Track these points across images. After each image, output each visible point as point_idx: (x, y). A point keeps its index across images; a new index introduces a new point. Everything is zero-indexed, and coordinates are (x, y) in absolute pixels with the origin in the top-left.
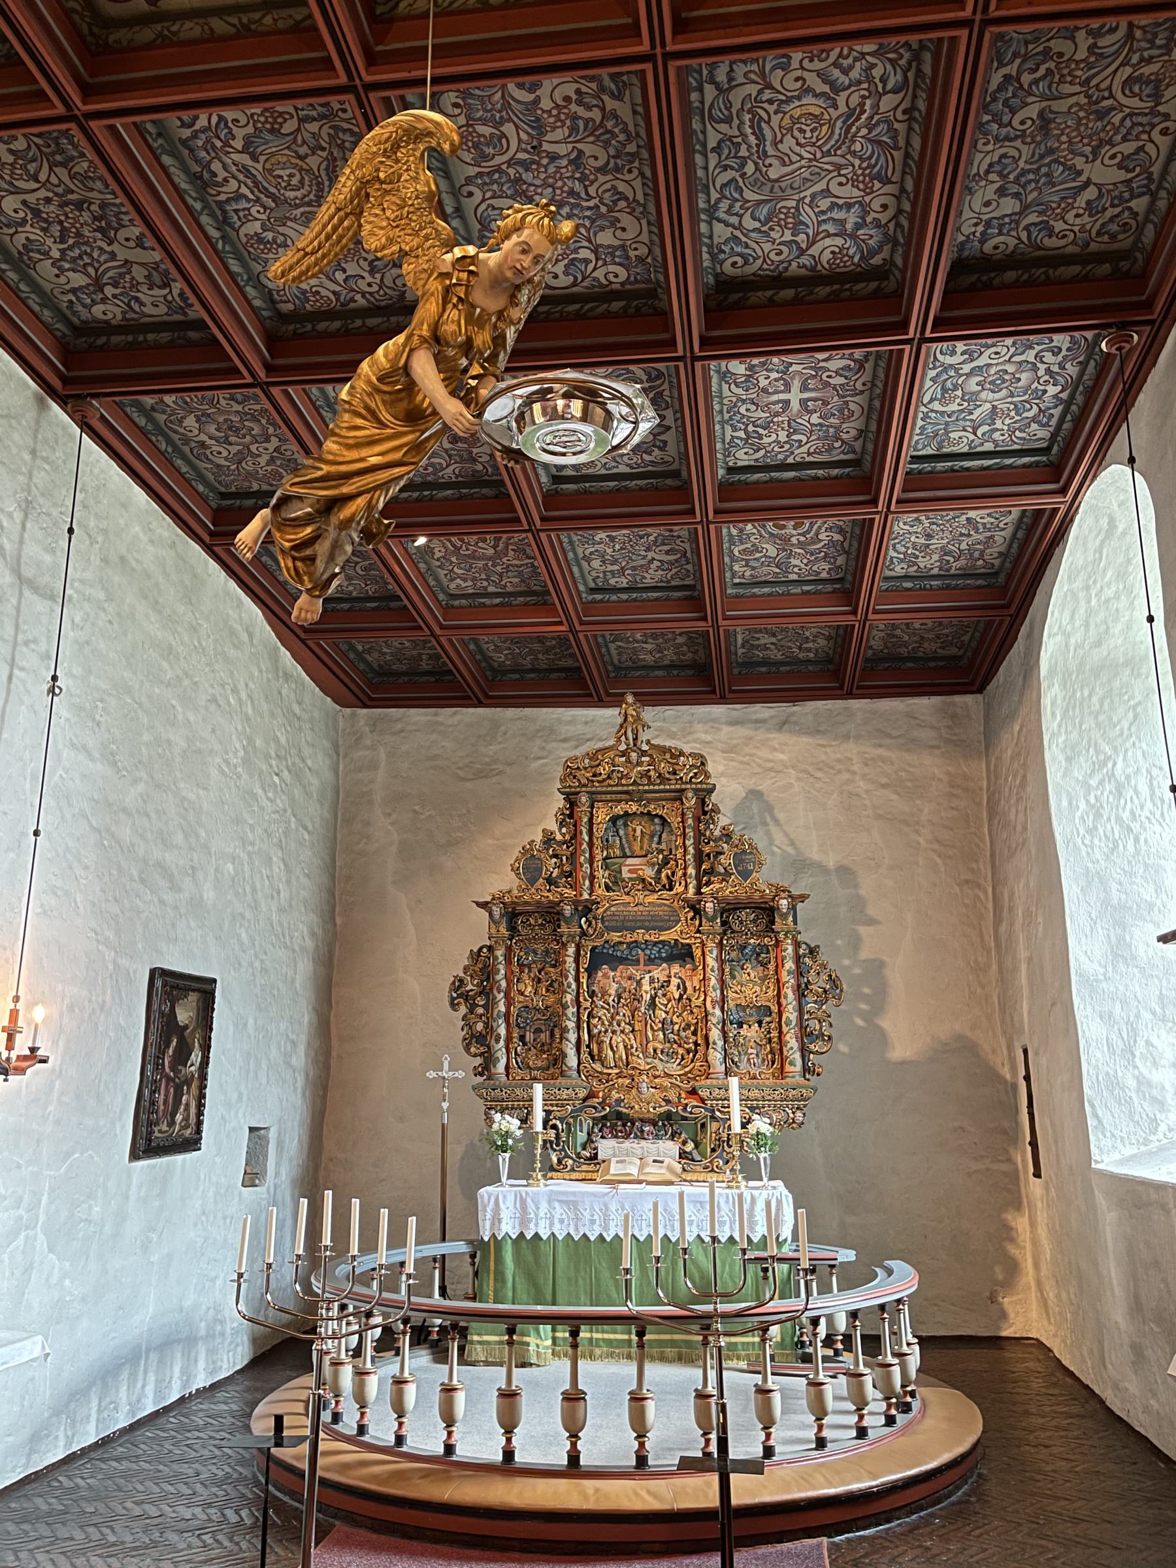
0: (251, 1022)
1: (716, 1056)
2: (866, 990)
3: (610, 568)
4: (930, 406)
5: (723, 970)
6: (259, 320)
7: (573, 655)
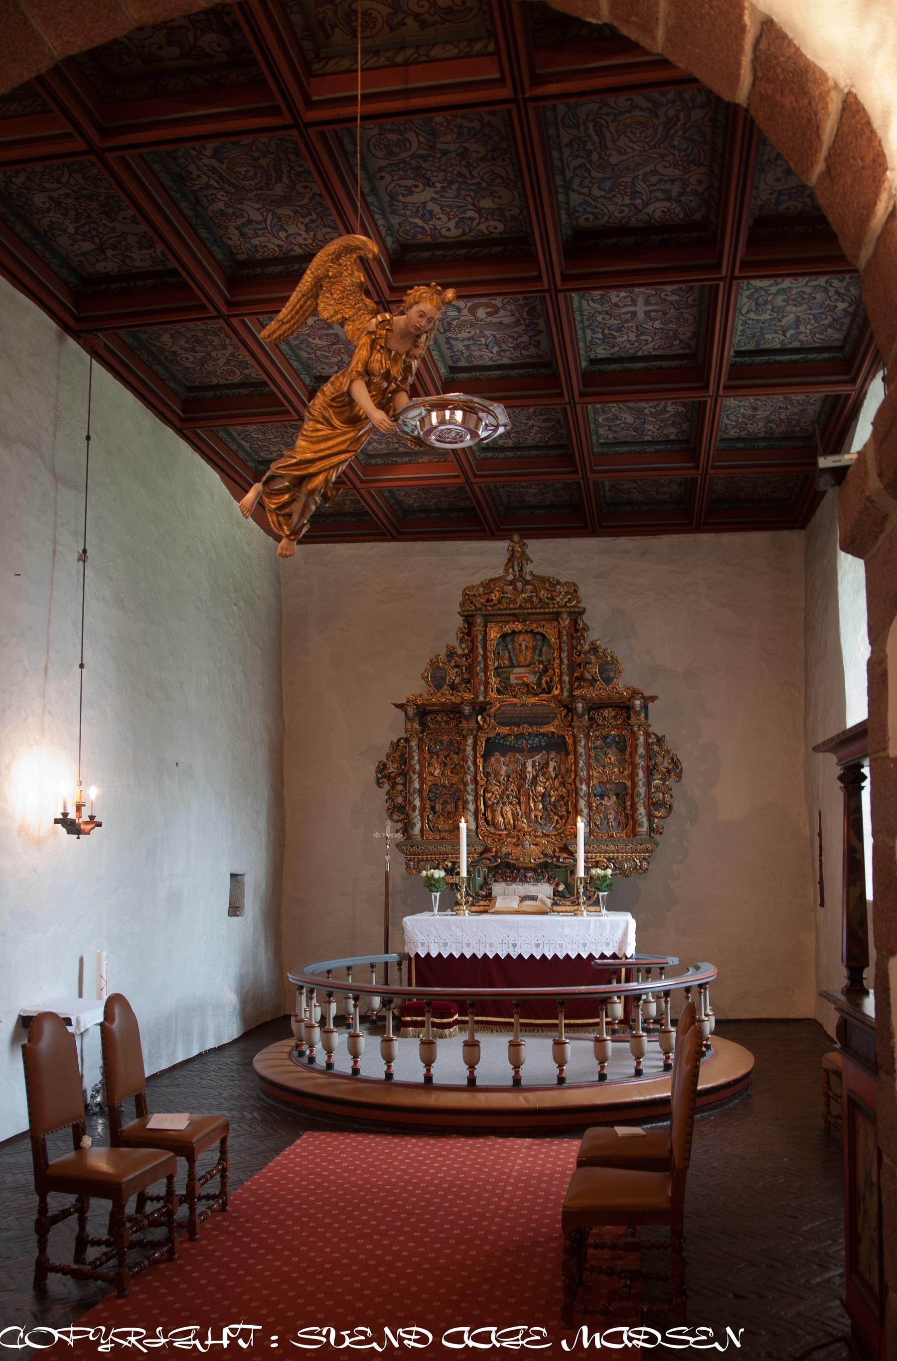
4: (748, 316)
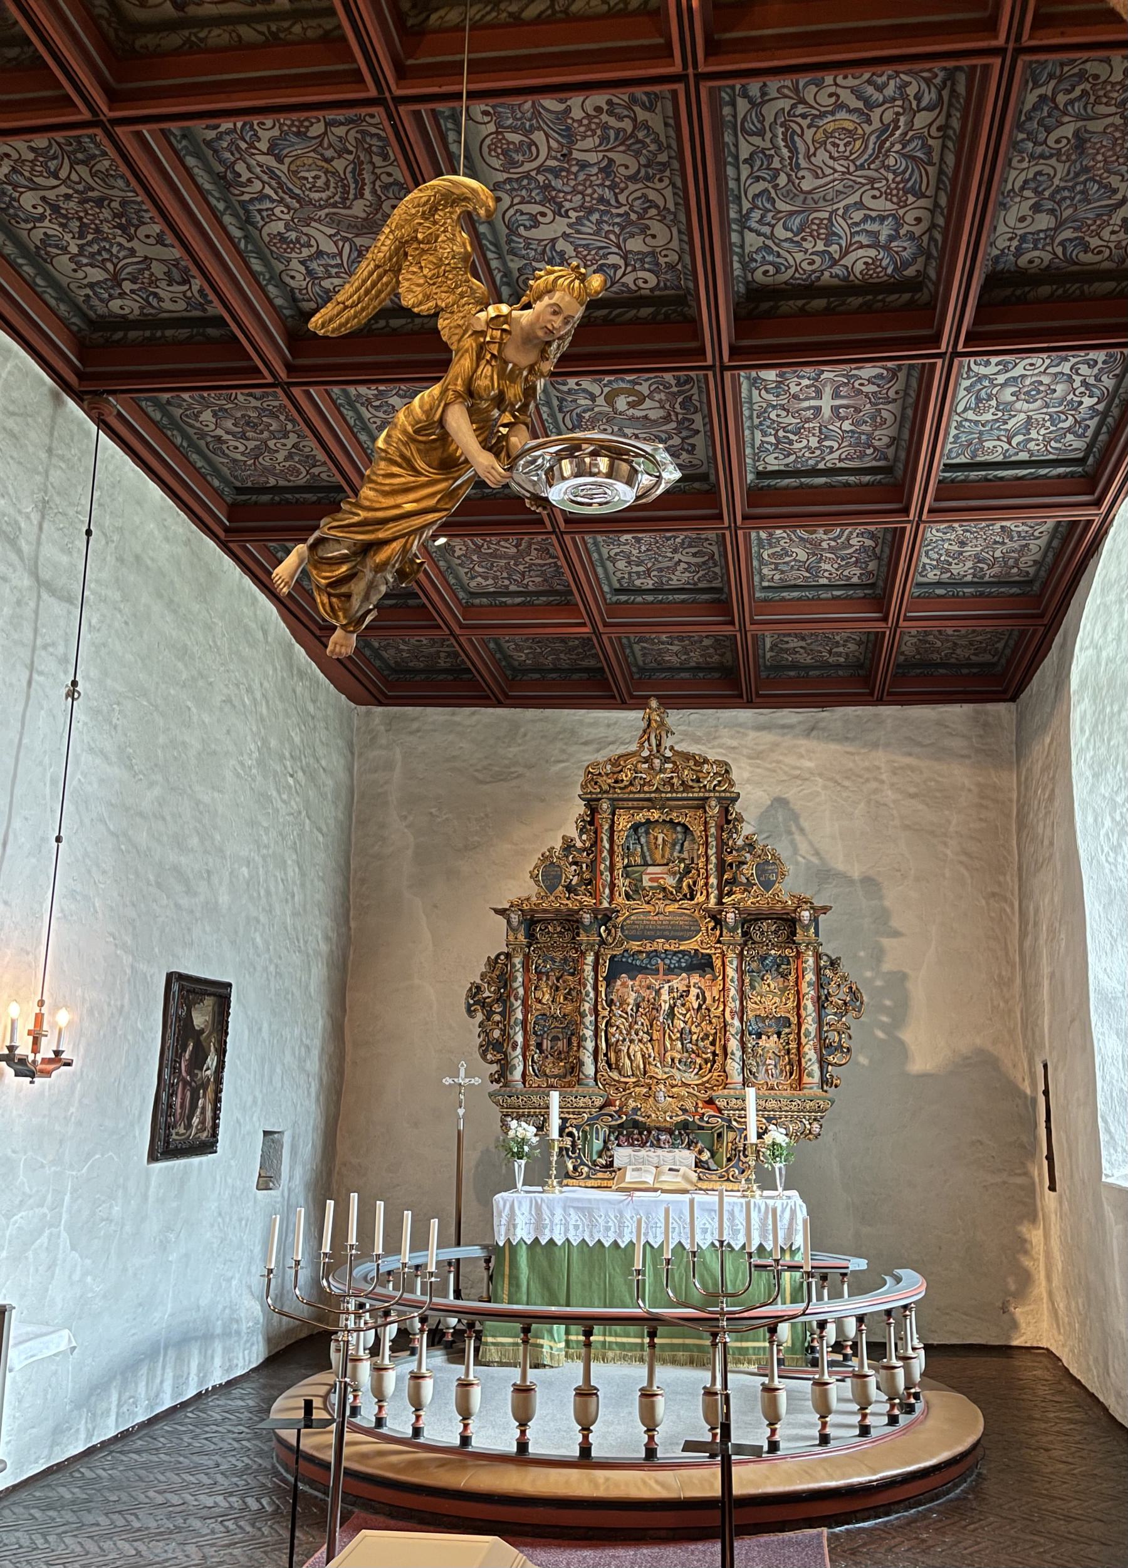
0: (265, 1026)
1: (734, 1067)
2: (888, 1003)
3: (635, 569)
4: (964, 415)
5: (743, 981)
6: (280, 318)
7: (596, 655)
